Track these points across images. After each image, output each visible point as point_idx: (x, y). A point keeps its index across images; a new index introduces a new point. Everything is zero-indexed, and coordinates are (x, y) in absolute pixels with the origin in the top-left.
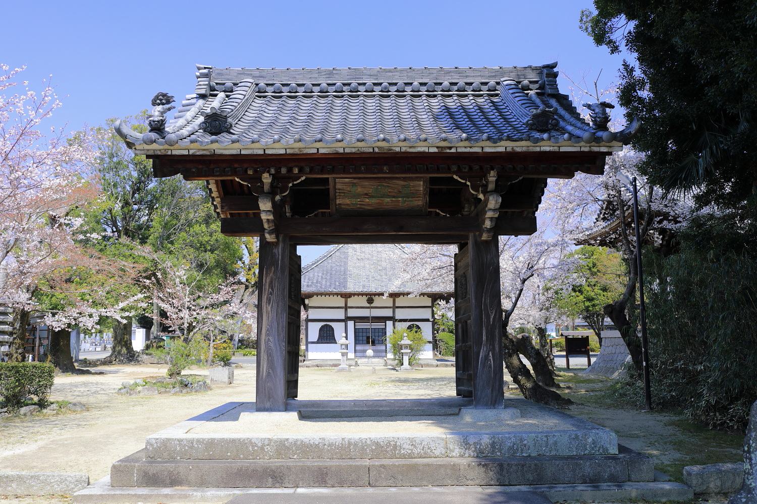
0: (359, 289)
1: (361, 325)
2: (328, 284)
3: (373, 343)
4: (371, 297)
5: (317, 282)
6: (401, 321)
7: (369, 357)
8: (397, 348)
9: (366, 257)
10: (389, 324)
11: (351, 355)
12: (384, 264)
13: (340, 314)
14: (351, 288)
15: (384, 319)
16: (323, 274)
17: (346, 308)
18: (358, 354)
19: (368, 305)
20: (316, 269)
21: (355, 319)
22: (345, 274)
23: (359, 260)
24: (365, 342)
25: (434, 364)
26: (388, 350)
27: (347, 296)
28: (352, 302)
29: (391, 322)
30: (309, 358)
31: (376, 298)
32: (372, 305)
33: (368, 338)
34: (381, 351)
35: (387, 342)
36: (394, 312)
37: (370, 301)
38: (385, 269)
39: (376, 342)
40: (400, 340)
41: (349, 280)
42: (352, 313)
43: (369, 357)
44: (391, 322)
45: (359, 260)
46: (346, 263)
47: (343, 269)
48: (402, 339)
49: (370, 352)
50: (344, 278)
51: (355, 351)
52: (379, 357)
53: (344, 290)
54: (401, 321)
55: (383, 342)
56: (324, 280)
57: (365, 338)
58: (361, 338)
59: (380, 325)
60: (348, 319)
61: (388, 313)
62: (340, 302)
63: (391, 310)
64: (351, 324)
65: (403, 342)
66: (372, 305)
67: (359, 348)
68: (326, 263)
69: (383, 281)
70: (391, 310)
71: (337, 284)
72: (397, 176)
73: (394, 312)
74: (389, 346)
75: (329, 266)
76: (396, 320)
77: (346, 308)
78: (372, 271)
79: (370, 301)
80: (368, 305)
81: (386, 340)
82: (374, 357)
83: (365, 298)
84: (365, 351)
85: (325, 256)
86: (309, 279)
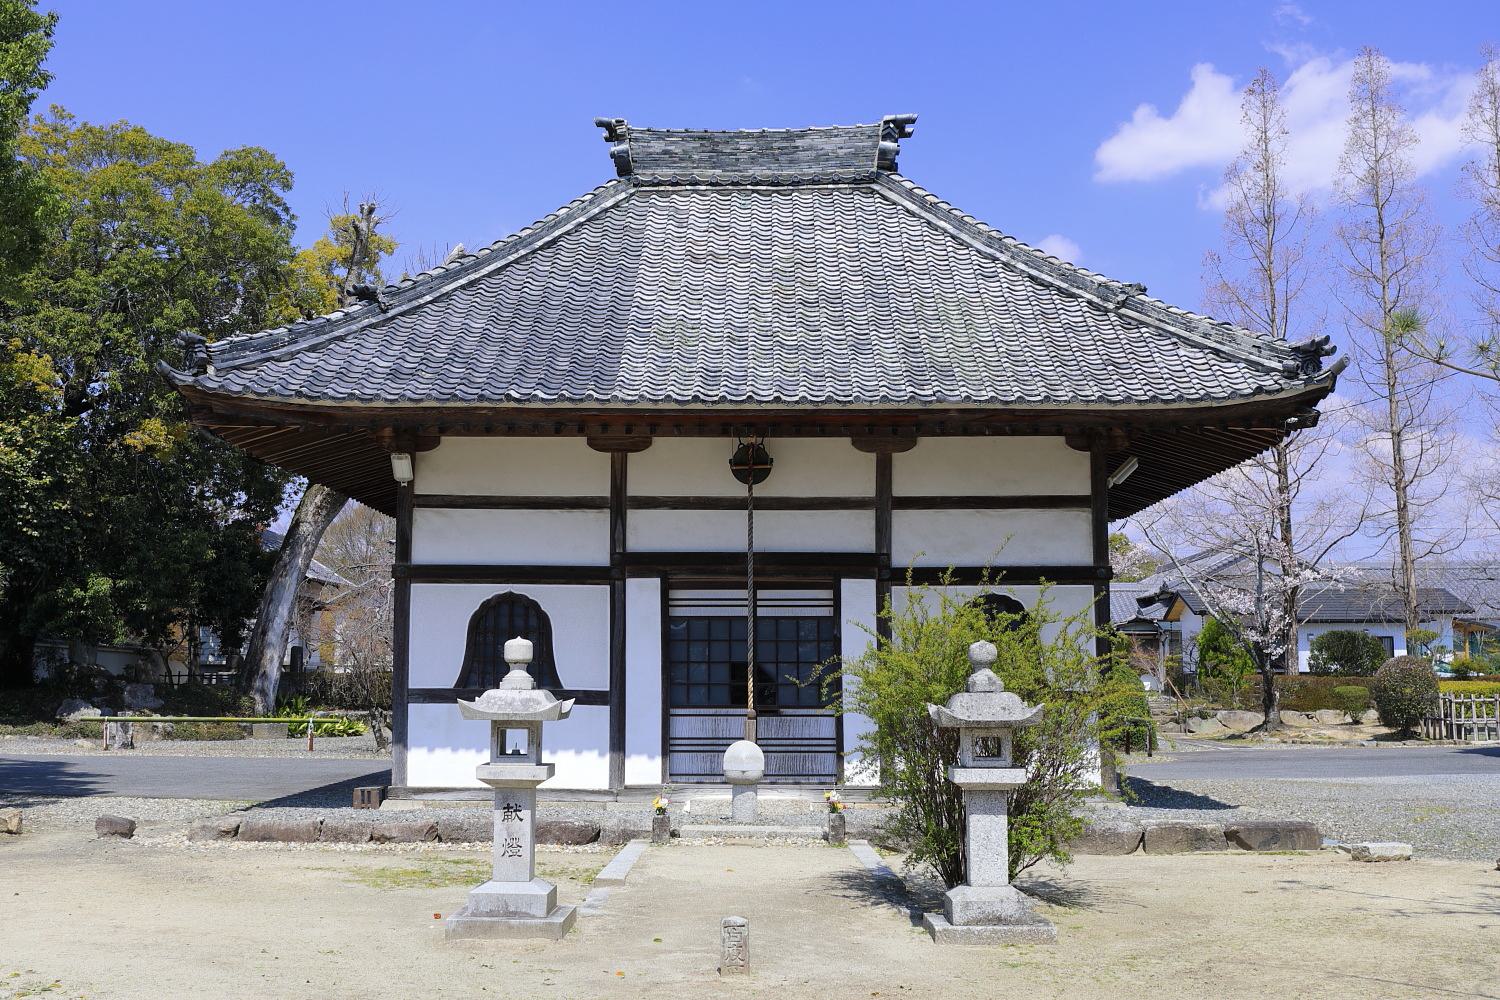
0: (681, 387)
1: (700, 603)
2: (511, 364)
3: (769, 705)
4: (753, 434)
5: (450, 359)
6: (928, 576)
7: (742, 785)
8: (922, 742)
9: (739, 247)
10: (858, 594)
11: (644, 768)
12: (829, 279)
13: (584, 540)
14: (640, 379)
15: (826, 569)
16: (494, 320)
17: (619, 504)
18: (683, 762)
19: (739, 490)
20: (462, 301)
21: (675, 569)
22: (613, 318)
23: (695, 259)
24: (723, 693)
25: (1125, 827)
26: (849, 743)
27: (623, 431)
28: (647, 473)
29: (870, 585)
30: (412, 782)
31: (785, 450)
32: (761, 490)
33: (738, 671)
34: (811, 746)
35: (849, 700)
36: (883, 530)
37: (751, 466)
38: (835, 299)
39: (784, 694)
40: (939, 689)
41: (629, 347)
42: (649, 532)
43: (742, 785)
44: (870, 585)
45: (695, 259)
46: (624, 275)
47: (604, 299)
48: (958, 681)
49: (745, 756)
50: (606, 339)
51: (668, 747)
52: (796, 777)
53: (592, 395)
54: (928, 576)
55: (825, 695)
56: (492, 351)
57: (722, 673)
58: (700, 672)
59: (802, 603)
60: (624, 565)
61: (852, 533)
62: (589, 472)
63: (868, 518)
64: (644, 595)
65: (964, 708)
66: (761, 490)
67: (687, 725)
68: (518, 274)
69: (820, 354)
70: (868, 518)
71: (563, 363)
72: (771, 580)
73: (883, 530)
74: (859, 727)
75: (534, 290)
76: (898, 576)
77: (619, 504)
78: (767, 307)
79: (751, 466)
80: (739, 490)
81: (837, 685)
82: (772, 777)
83: (724, 448)
84: (717, 745)
85: (520, 242)
86: (410, 344)
